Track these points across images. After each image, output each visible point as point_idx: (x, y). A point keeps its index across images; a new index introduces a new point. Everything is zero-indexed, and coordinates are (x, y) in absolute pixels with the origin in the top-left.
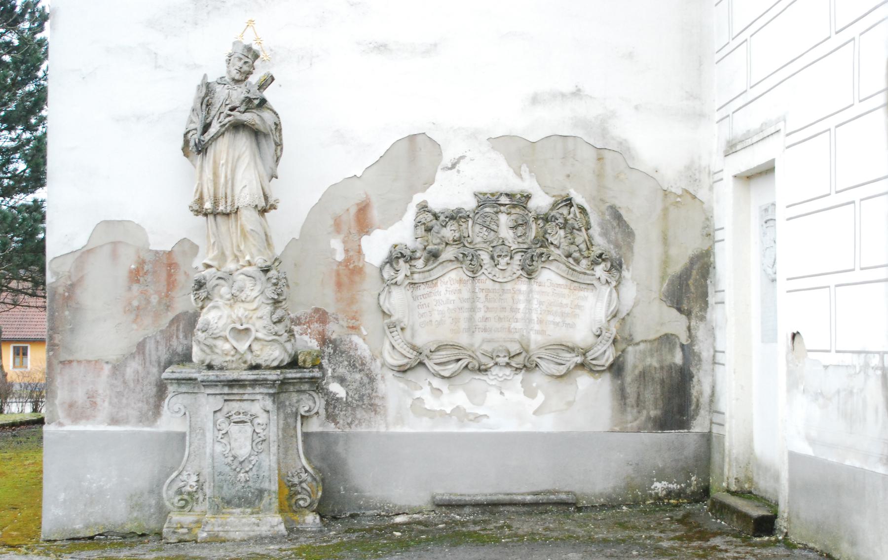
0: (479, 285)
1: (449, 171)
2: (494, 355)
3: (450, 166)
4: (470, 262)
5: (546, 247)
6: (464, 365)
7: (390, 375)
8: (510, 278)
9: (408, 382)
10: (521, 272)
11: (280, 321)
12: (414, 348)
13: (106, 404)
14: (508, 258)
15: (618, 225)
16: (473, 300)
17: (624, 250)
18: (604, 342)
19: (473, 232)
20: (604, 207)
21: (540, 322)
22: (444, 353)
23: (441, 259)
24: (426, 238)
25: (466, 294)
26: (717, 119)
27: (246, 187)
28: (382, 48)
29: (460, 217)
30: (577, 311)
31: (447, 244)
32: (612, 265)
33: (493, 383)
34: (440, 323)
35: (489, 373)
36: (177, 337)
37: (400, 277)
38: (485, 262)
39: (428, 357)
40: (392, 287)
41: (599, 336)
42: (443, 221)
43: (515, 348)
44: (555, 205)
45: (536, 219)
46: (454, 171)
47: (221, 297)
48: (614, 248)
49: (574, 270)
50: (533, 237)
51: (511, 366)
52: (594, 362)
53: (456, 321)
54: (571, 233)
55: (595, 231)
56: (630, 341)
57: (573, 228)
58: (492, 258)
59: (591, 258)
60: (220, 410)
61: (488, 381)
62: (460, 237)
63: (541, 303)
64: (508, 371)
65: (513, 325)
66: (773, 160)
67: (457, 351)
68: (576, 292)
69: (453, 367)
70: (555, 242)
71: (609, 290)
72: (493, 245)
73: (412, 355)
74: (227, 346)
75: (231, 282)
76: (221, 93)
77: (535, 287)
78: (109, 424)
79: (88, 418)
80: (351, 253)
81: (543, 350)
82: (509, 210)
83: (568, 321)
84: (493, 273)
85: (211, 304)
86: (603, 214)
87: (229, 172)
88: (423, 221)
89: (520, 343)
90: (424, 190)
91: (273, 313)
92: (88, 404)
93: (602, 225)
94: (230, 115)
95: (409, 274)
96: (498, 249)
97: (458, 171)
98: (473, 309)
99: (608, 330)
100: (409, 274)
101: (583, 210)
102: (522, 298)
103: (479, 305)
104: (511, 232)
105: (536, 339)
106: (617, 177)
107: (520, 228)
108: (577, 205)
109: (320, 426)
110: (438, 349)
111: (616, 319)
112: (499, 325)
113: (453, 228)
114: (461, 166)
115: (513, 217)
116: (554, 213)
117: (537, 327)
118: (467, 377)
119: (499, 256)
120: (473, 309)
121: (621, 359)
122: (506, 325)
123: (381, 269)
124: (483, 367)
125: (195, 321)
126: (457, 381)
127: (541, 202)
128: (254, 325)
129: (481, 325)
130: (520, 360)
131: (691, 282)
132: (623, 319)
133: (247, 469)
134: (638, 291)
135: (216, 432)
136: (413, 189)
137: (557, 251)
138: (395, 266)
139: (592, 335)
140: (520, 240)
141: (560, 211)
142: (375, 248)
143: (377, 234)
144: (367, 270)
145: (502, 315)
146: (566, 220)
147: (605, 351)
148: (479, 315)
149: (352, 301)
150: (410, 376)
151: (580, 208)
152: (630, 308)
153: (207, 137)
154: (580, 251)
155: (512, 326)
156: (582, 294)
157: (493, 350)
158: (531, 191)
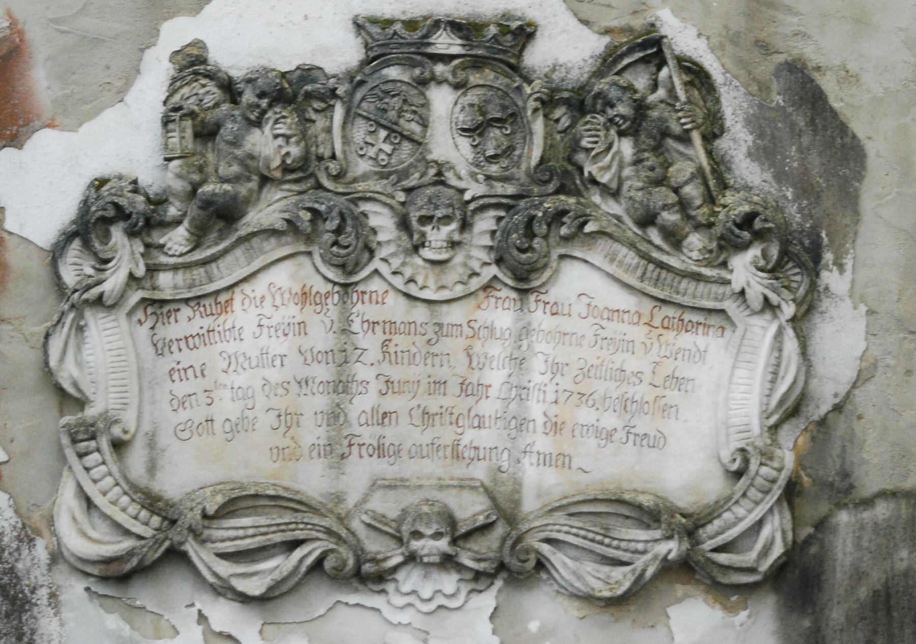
0: (363, 310)
2: (406, 529)
4: (337, 240)
5: (578, 193)
6: (310, 560)
7: (75, 589)
8: (459, 290)
9: (133, 611)
10: (494, 270)
12: (151, 502)
14: (454, 226)
15: (812, 122)
16: (343, 356)
17: (828, 202)
18: (753, 493)
19: (346, 140)
20: (766, 68)
21: (555, 427)
24: (197, 161)
25: (321, 337)
29: (309, 96)
30: (673, 396)
31: (265, 180)
32: (784, 253)
33: (405, 617)
34: (236, 428)
35: (390, 587)
37: (113, 282)
38: (381, 237)
40: (88, 313)
42: (253, 106)
43: (470, 508)
44: (608, 62)
45: (548, 103)
48: (797, 197)
49: (661, 265)
50: (534, 162)
51: (460, 568)
52: (723, 558)
53: (288, 420)
54: (658, 149)
55: (737, 142)
56: (843, 491)
57: (665, 133)
58: (404, 224)
59: (718, 230)
61: (387, 612)
62: (305, 159)
63: (556, 368)
64: (449, 582)
65: (469, 436)
67: (288, 517)
68: (670, 335)
69: (277, 566)
70: (604, 179)
71: (773, 329)
73: (145, 526)
77: (539, 317)
81: (560, 518)
82: (461, 75)
83: (643, 425)
84: (408, 272)
86: (764, 88)
88: (191, 104)
89: (489, 493)
93: (758, 124)
95: (140, 271)
96: (421, 200)
99: (767, 456)
100: (140, 271)
101: (696, 75)
102: (497, 350)
103: (362, 372)
104: (465, 143)
105: (539, 485)
110: (230, 509)
111: (800, 423)
113: (282, 129)
115: (473, 97)
116: (601, 85)
117: (543, 443)
118: (320, 599)
119: (426, 220)
120: (342, 386)
121: (813, 550)
122: (447, 435)
123: (57, 253)
124: (367, 568)
126: (290, 611)
127: (565, 48)
129: (368, 435)
130: (488, 544)
132: (822, 422)
133: (195, 97)
134: (870, 334)
137: (613, 207)
138: (97, 245)
139: (719, 473)
140: (494, 169)
141: (628, 77)
143: (44, 143)
146: (641, 108)
148: (362, 404)
150: (143, 595)
151: (688, 70)
152: (843, 390)
154: (683, 205)
155: (465, 440)
156: (687, 340)
158: (533, 14)
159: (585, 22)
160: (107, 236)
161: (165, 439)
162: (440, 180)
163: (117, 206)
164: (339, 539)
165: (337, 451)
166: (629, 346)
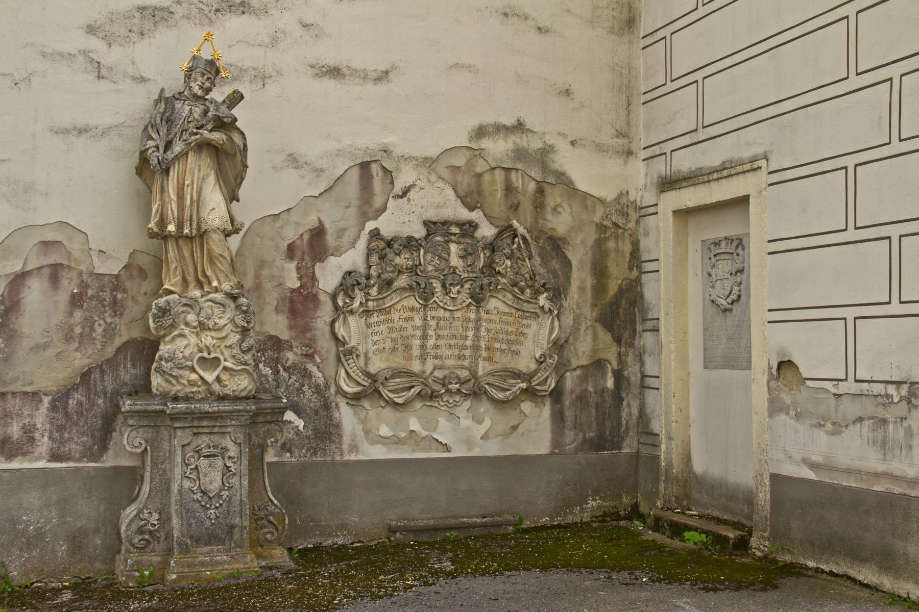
1: (400, 200)
3: (400, 193)
10: (470, 300)
11: (249, 350)
12: (368, 375)
13: (46, 439)
19: (425, 260)
21: (488, 349)
22: (398, 380)
26: (643, 158)
27: (215, 208)
28: (335, 72)
30: (522, 338)
31: (399, 272)
36: (125, 366)
37: (356, 304)
38: (437, 290)
39: (382, 384)
41: (542, 363)
46: (405, 199)
47: (187, 324)
52: (537, 387)
58: (444, 286)
60: (188, 444)
63: (488, 331)
66: (749, 196)
74: (194, 377)
75: (198, 309)
76: (183, 109)
78: (49, 461)
79: (24, 455)
80: (305, 280)
83: (513, 348)
85: (176, 333)
87: (195, 194)
90: (376, 218)
91: (242, 341)
92: (25, 441)
94: (196, 134)
95: (364, 301)
96: (450, 277)
97: (409, 200)
98: (425, 337)
101: (524, 239)
103: (431, 333)
104: (461, 260)
106: (555, 210)
107: (470, 258)
109: (276, 456)
112: (449, 353)
113: (407, 256)
114: (412, 194)
115: (462, 246)
119: (451, 285)
120: (425, 337)
125: (157, 349)
127: (487, 231)
128: (222, 354)
129: (432, 352)
131: (621, 310)
132: (562, 346)
135: (185, 468)
136: (365, 217)
137: (504, 280)
142: (329, 276)
143: (332, 260)
144: (323, 297)
145: (452, 342)
147: (547, 378)
148: (431, 342)
149: (307, 328)
153: (170, 155)
157: (445, 377)
159: (491, 223)
160: (353, 291)
161: (370, 355)
162: (454, 272)
163: (357, 281)
164: (426, 385)
165: (423, 358)
166: (508, 323)
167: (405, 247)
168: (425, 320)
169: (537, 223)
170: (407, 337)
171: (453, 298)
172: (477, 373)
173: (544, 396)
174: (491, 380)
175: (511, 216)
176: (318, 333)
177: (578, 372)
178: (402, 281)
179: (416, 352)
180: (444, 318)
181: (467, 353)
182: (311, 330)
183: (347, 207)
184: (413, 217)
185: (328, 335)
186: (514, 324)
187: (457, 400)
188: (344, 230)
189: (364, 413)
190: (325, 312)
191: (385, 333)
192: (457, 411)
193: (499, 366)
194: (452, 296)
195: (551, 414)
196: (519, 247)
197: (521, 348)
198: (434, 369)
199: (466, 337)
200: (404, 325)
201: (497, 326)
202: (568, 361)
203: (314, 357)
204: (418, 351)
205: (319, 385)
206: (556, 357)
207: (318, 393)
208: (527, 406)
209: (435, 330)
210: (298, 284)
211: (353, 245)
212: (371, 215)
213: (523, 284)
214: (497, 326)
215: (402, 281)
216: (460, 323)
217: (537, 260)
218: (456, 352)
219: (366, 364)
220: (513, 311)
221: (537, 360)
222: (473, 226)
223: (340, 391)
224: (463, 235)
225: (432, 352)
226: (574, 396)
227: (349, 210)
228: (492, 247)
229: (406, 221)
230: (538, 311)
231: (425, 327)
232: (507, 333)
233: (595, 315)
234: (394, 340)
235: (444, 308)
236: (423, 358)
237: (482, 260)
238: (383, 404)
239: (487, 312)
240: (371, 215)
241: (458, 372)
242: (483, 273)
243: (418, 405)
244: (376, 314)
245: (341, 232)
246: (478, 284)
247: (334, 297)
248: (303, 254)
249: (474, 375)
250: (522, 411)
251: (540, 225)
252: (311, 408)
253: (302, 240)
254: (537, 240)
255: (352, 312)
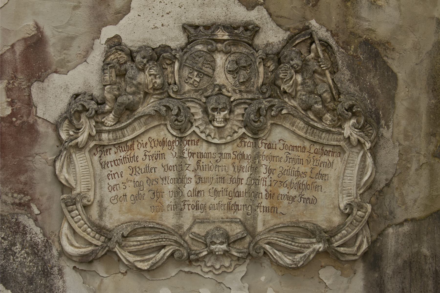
5: (278, 97)
7: (68, 270)
10: (244, 130)
12: (100, 230)
19: (180, 77)
21: (270, 195)
23: (137, 114)
30: (319, 181)
31: (146, 94)
32: (366, 121)
37: (82, 138)
39: (120, 245)
41: (348, 215)
49: (314, 127)
52: (342, 249)
58: (205, 111)
62: (163, 84)
63: (270, 171)
72: (206, 94)
84: (208, 131)
90: (115, 22)
96: (213, 100)
98: (180, 180)
101: (326, 45)
103: (189, 174)
104: (230, 76)
107: (243, 72)
108: (320, 40)
113: (153, 72)
115: (232, 57)
117: (265, 203)
119: (214, 109)
120: (180, 180)
127: (272, 36)
129: (191, 200)
132: (381, 191)
136: (100, 21)
137: (294, 103)
142: (51, 98)
144: (42, 128)
145: (219, 187)
147: (357, 235)
148: (189, 187)
159: (279, 26)
162: (220, 93)
163: (83, 106)
164: (181, 245)
165: (179, 209)
166: (300, 161)
167: (151, 59)
168: (181, 157)
169: (346, 22)
170: (156, 180)
171: (218, 128)
172: (255, 228)
173: (355, 261)
174: (274, 238)
175: (308, 14)
176: (37, 175)
177: (406, 228)
178: (148, 106)
179: (168, 200)
180: (208, 155)
181: (241, 201)
182: (26, 171)
183: (75, 8)
184: (166, 20)
185: (50, 178)
186: (308, 162)
187: (227, 264)
188: (72, 38)
189: (97, 281)
190: (46, 147)
191: (126, 175)
192: (228, 280)
193: (286, 220)
194: (216, 124)
195: (365, 286)
196: (317, 56)
197: (320, 195)
198: (194, 223)
199: (239, 180)
200: (152, 164)
201: (283, 164)
202: (391, 213)
203: (29, 207)
204: (172, 199)
205: (36, 244)
206: (369, 207)
207: (35, 254)
208: (328, 274)
209: (195, 170)
210: (9, 111)
211: (84, 58)
212: (109, 18)
213: (319, 106)
214: (283, 164)
215: (148, 106)
216: (230, 161)
217: (345, 74)
218: (225, 200)
219: (101, 216)
220: (307, 144)
221: (342, 213)
222: (253, 30)
223: (62, 252)
224: (235, 42)
225: (191, 200)
226: (400, 261)
227: (78, 12)
228: (278, 58)
229: (159, 25)
230: (342, 143)
231: (180, 167)
232: (298, 174)
233: (432, 148)
234: (138, 184)
235: (207, 142)
236: (179, 209)
237: (261, 75)
238: (123, 270)
239: (269, 146)
240: (109, 18)
241: (227, 227)
242: (263, 93)
243: (172, 271)
244: (113, 150)
245: (67, 42)
246: (254, 107)
247: (56, 127)
248: (15, 71)
249: (250, 231)
250: (321, 281)
251: (350, 25)
252: (23, 275)
253: (14, 52)
254: (345, 45)
255: (78, 148)
